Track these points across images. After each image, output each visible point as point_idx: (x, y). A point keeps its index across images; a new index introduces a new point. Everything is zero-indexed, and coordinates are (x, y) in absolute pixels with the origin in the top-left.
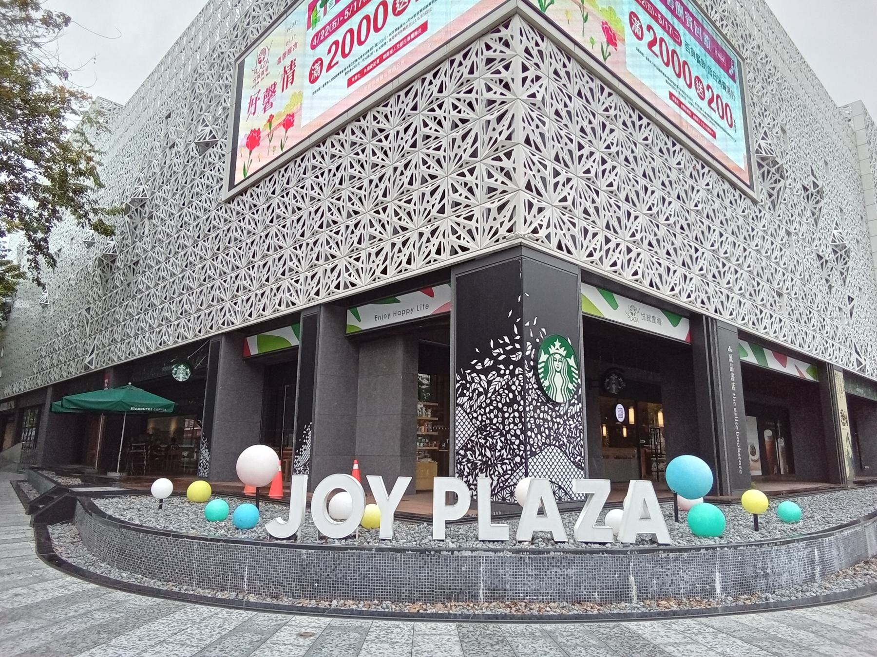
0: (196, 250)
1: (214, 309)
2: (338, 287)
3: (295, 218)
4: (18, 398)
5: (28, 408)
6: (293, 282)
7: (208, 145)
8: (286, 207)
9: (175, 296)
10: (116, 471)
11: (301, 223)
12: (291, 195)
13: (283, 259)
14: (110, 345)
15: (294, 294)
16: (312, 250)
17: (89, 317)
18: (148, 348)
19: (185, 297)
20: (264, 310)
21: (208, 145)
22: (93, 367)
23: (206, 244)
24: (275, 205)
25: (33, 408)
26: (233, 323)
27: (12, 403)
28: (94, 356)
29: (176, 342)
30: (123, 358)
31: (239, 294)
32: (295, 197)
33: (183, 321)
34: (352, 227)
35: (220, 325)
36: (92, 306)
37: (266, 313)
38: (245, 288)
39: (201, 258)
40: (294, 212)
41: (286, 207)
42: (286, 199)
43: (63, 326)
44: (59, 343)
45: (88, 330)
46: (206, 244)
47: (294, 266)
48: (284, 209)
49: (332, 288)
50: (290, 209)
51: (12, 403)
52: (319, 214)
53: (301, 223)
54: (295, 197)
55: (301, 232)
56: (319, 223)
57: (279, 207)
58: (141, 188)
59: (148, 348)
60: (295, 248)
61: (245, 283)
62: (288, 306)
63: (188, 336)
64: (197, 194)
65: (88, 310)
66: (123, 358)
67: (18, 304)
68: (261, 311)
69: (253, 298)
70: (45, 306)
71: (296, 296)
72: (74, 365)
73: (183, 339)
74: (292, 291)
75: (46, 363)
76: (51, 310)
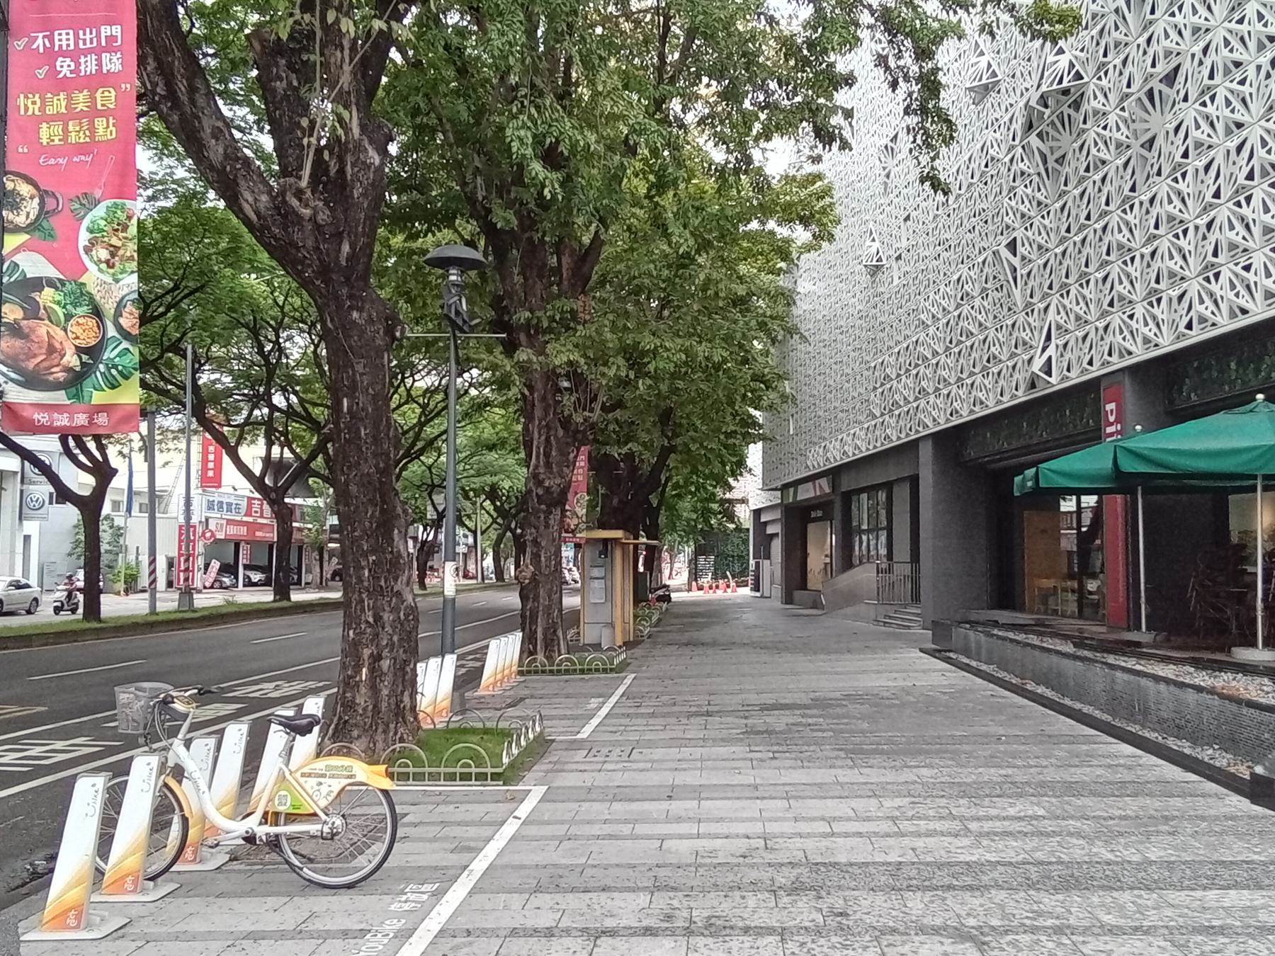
0: (1029, 234)
1: (1019, 360)
2: (1189, 326)
3: (1232, 144)
4: (834, 474)
5: (863, 490)
6: (1238, 269)
7: (986, 89)
8: (1212, 124)
9: (1091, 269)
10: (1254, 644)
11: (1213, 173)
12: (1220, 100)
13: (1109, 280)
14: (916, 399)
15: (1243, 292)
16: (1204, 238)
17: (1016, 261)
18: (934, 420)
19: (1115, 270)
20: (1068, 370)
21: (986, 89)
22: (1053, 380)
23: (1046, 222)
24: (1189, 122)
25: (871, 489)
26: (1130, 353)
27: (824, 482)
28: (1051, 351)
29: (972, 412)
30: (942, 421)
31: (1162, 286)
32: (1228, 103)
33: (1116, 320)
34: (1199, 55)
35: (1085, 365)
36: (1019, 234)
37: (1073, 374)
38: (1172, 275)
39: (1040, 247)
40: (1228, 132)
41: (1212, 124)
42: (1210, 109)
43: (944, 297)
44: (932, 338)
45: (1017, 293)
46: (1046, 222)
47: (1239, 239)
48: (1208, 130)
49: (1182, 329)
50: (1220, 127)
51: (824, 482)
52: (1245, 153)
53: (1213, 173)
54: (1228, 103)
55: (1213, 189)
56: (1246, 171)
57: (1198, 127)
58: (983, 62)
59: (934, 420)
60: (1239, 204)
61: (1232, 235)
62: (1233, 315)
63: (1133, 349)
64: (1117, 44)
65: (1012, 246)
66: (942, 421)
67: (804, 286)
68: (1106, 356)
69: (1092, 335)
70: (875, 270)
71: (1247, 297)
72: (893, 421)
73: (1121, 356)
74: (1239, 287)
75: (904, 388)
76: (895, 273)
